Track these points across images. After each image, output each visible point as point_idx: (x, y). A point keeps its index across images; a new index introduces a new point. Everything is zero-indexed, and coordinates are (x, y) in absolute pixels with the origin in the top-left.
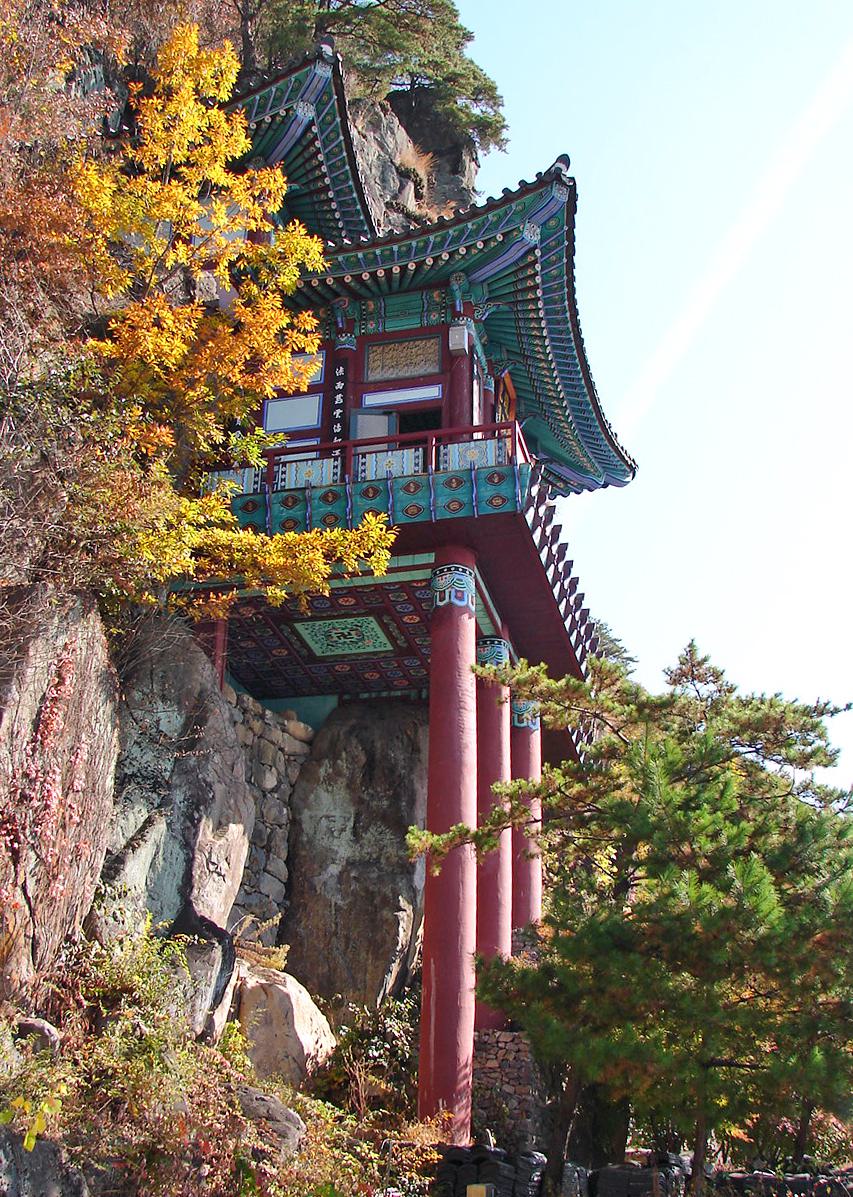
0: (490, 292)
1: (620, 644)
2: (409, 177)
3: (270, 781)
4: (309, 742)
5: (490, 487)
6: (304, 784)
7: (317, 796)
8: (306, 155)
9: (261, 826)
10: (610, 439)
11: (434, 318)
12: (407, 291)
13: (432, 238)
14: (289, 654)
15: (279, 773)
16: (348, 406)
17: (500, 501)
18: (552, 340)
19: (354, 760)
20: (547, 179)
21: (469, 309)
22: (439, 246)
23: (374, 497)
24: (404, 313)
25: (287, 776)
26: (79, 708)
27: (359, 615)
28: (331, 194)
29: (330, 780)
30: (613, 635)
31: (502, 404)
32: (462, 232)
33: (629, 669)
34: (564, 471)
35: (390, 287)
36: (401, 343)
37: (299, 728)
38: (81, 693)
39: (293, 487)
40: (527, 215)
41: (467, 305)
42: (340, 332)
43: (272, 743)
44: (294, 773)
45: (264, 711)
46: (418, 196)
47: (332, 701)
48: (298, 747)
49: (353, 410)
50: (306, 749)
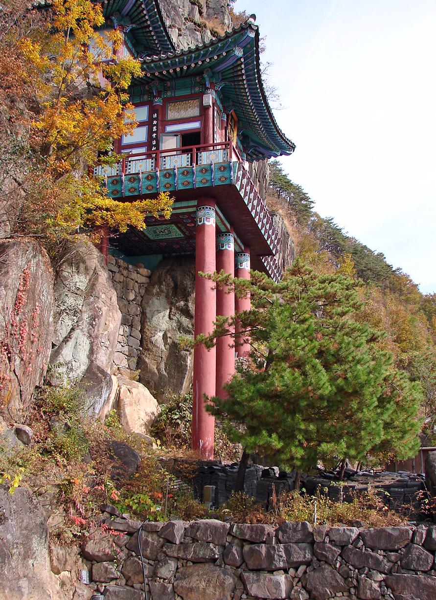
0: (223, 76)
1: (307, 195)
2: (196, 4)
3: (132, 296)
4: (149, 277)
5: (219, 173)
6: (147, 296)
7: (153, 302)
8: (138, 11)
9: (128, 317)
10: (281, 136)
11: (197, 90)
12: (184, 77)
13: (193, 55)
14: (139, 239)
15: (136, 292)
16: (159, 132)
17: (224, 179)
18: (252, 96)
19: (168, 285)
20: (245, 27)
21: (213, 86)
22: (196, 58)
23: (169, 177)
24: (184, 87)
25: (140, 293)
26: (34, 293)
27: (167, 224)
28: (151, 29)
29: (158, 294)
30: (304, 191)
31: (231, 125)
32: (207, 52)
33: (311, 206)
34: (262, 150)
35: (177, 76)
36: (182, 101)
37: (145, 271)
38: (35, 285)
39: (134, 172)
40: (236, 43)
41: (212, 83)
42: (155, 97)
43: (132, 280)
44: (143, 291)
45: (128, 265)
46: (201, 13)
47: (160, 257)
48: (144, 280)
49: (161, 134)
50: (147, 280)
